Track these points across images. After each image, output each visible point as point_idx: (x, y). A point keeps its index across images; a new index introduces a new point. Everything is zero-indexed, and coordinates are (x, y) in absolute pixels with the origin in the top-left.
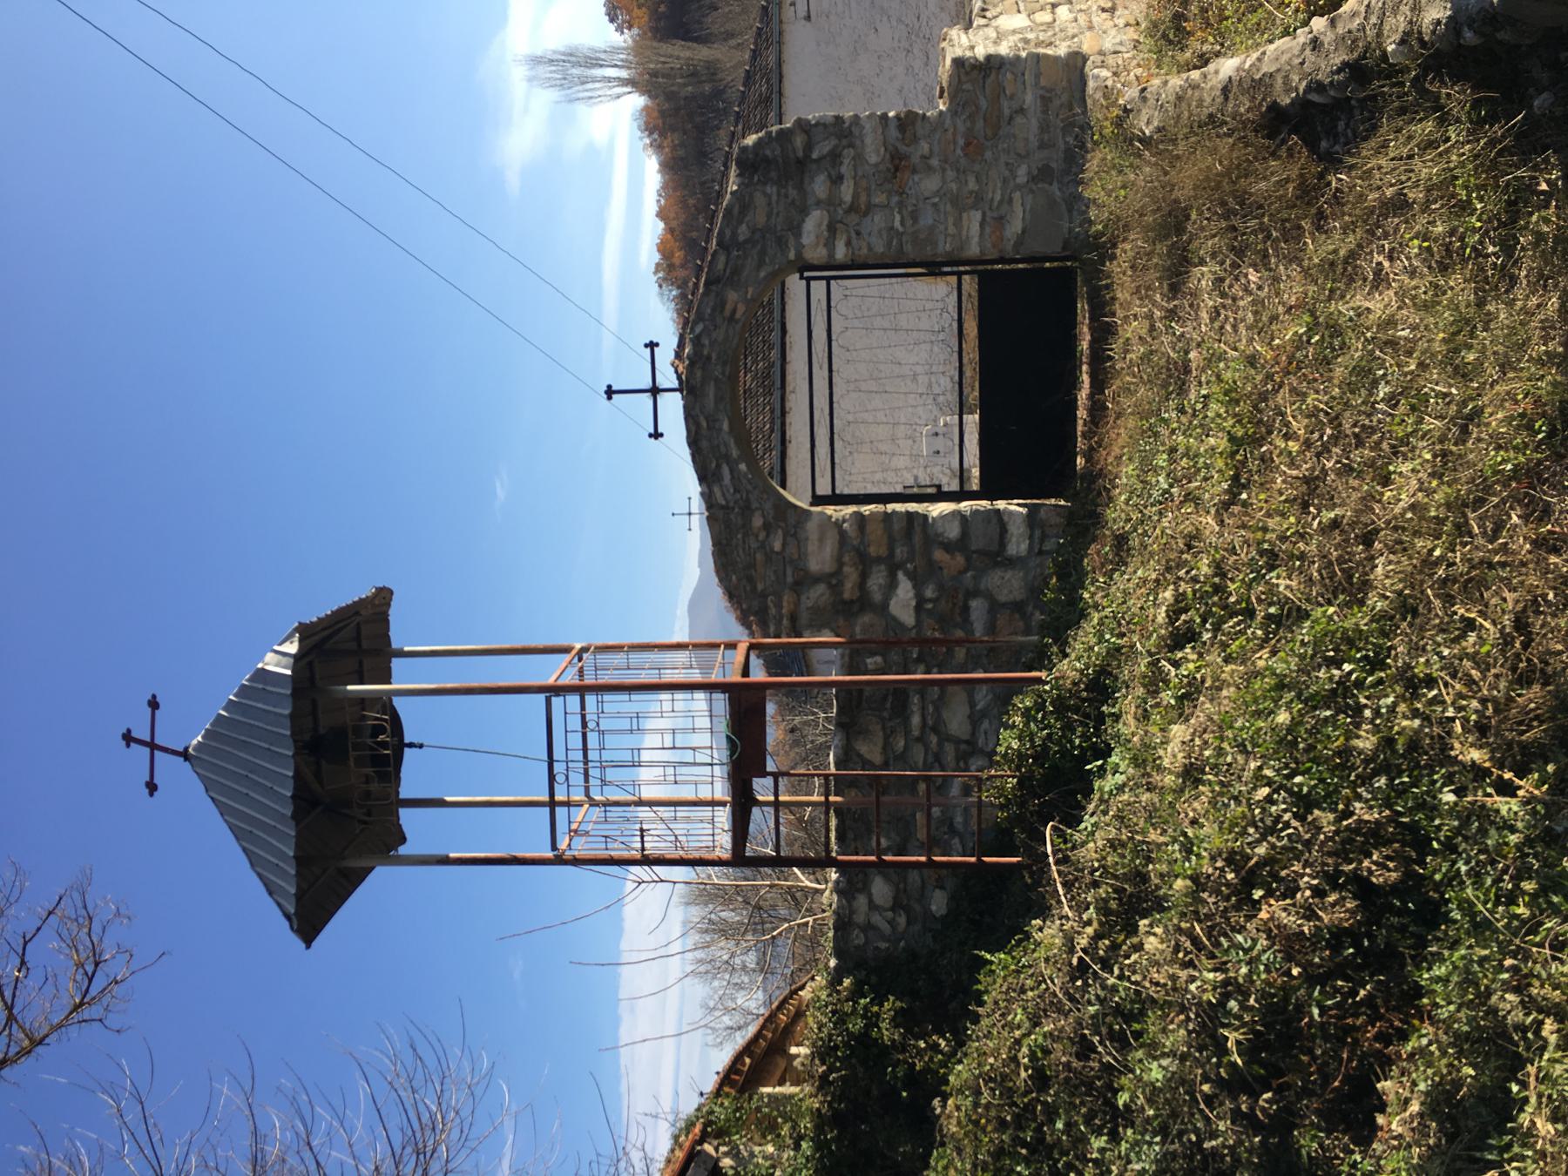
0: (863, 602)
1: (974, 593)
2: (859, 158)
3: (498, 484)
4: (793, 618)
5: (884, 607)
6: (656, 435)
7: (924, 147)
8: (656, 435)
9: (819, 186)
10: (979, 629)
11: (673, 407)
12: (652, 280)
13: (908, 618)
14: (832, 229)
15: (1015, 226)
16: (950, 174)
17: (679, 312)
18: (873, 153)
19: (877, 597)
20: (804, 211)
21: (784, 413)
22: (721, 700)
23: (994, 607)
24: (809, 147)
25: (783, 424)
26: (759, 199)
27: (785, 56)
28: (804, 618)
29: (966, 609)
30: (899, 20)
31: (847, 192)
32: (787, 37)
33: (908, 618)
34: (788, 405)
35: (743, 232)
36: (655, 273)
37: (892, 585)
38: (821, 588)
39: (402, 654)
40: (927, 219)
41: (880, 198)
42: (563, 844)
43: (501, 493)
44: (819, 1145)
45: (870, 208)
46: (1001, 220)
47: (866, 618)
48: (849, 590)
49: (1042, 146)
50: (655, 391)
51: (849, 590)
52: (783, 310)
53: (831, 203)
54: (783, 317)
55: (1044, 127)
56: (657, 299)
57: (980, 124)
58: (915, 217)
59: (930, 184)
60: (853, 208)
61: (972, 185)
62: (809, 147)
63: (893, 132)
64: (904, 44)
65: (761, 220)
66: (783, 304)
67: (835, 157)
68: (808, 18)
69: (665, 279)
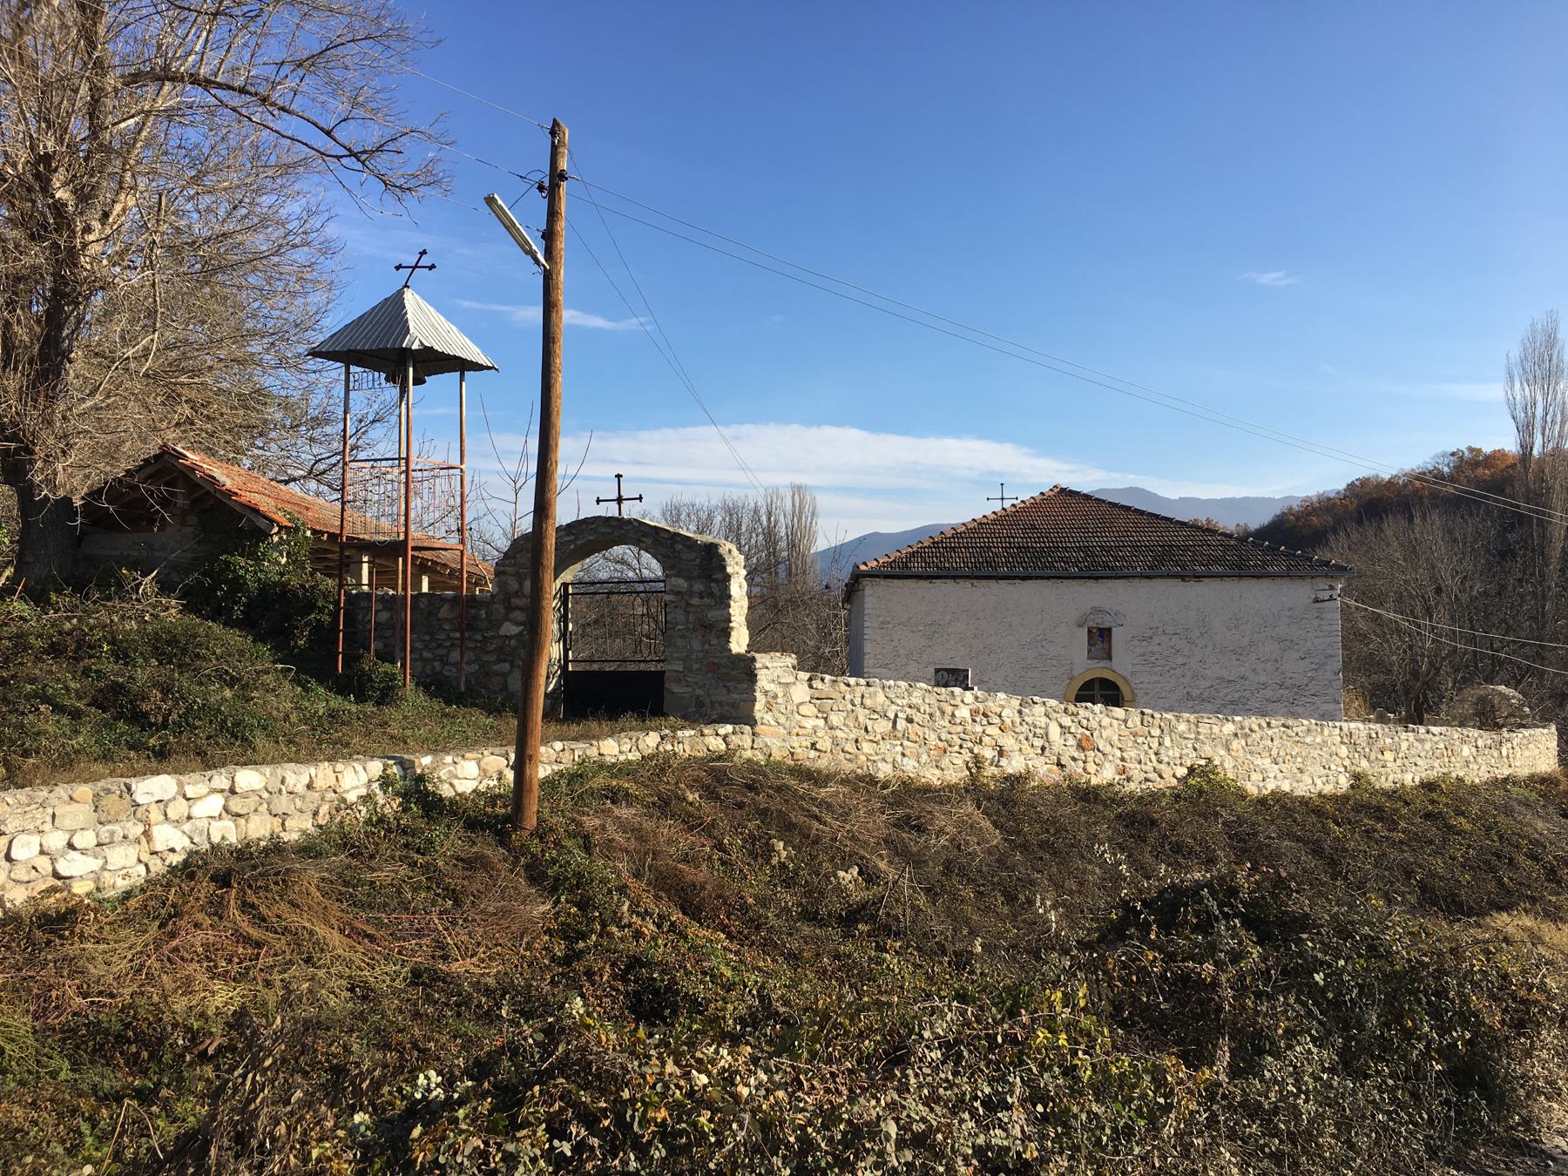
0: (510, 609)
1: (512, 663)
2: (710, 607)
3: (1279, 274)
4: (504, 573)
5: (506, 619)
6: (598, 501)
7: (714, 642)
8: (598, 501)
9: (698, 587)
10: (496, 668)
11: (611, 510)
12: (1461, 442)
13: (502, 632)
14: (678, 593)
15: (676, 689)
16: (701, 655)
17: (1420, 477)
18: (712, 615)
19: (512, 616)
20: (688, 579)
21: (954, 578)
22: (402, 537)
23: (505, 675)
24: (717, 581)
25: (946, 577)
26: (693, 555)
27: (1136, 582)
28: (504, 578)
29: (505, 661)
30: (1312, 679)
31: (695, 601)
32: (1298, 583)
33: (502, 632)
34: (961, 581)
35: (678, 547)
36: (1471, 449)
37: (517, 624)
38: (516, 587)
39: (462, 379)
40: (680, 642)
41: (691, 618)
42: (353, 465)
43: (1267, 278)
44: (275, 584)
45: (687, 613)
46: (678, 681)
47: (502, 610)
48: (515, 601)
49: (712, 703)
50: (620, 500)
51: (515, 601)
52: (1042, 578)
53: (691, 594)
54: (1037, 578)
55: (721, 704)
56: (1439, 450)
57: (725, 670)
58: (683, 636)
59: (696, 644)
60: (688, 604)
61: (696, 666)
62: (717, 581)
63: (723, 625)
64: (1289, 682)
65: (684, 556)
66: (1048, 578)
67: (711, 595)
68: (1316, 601)
69: (1461, 458)
